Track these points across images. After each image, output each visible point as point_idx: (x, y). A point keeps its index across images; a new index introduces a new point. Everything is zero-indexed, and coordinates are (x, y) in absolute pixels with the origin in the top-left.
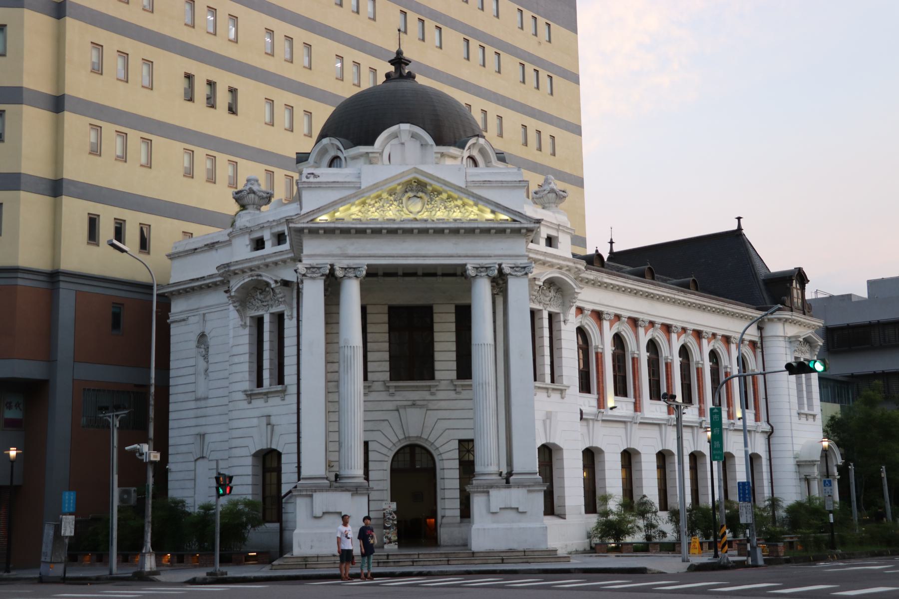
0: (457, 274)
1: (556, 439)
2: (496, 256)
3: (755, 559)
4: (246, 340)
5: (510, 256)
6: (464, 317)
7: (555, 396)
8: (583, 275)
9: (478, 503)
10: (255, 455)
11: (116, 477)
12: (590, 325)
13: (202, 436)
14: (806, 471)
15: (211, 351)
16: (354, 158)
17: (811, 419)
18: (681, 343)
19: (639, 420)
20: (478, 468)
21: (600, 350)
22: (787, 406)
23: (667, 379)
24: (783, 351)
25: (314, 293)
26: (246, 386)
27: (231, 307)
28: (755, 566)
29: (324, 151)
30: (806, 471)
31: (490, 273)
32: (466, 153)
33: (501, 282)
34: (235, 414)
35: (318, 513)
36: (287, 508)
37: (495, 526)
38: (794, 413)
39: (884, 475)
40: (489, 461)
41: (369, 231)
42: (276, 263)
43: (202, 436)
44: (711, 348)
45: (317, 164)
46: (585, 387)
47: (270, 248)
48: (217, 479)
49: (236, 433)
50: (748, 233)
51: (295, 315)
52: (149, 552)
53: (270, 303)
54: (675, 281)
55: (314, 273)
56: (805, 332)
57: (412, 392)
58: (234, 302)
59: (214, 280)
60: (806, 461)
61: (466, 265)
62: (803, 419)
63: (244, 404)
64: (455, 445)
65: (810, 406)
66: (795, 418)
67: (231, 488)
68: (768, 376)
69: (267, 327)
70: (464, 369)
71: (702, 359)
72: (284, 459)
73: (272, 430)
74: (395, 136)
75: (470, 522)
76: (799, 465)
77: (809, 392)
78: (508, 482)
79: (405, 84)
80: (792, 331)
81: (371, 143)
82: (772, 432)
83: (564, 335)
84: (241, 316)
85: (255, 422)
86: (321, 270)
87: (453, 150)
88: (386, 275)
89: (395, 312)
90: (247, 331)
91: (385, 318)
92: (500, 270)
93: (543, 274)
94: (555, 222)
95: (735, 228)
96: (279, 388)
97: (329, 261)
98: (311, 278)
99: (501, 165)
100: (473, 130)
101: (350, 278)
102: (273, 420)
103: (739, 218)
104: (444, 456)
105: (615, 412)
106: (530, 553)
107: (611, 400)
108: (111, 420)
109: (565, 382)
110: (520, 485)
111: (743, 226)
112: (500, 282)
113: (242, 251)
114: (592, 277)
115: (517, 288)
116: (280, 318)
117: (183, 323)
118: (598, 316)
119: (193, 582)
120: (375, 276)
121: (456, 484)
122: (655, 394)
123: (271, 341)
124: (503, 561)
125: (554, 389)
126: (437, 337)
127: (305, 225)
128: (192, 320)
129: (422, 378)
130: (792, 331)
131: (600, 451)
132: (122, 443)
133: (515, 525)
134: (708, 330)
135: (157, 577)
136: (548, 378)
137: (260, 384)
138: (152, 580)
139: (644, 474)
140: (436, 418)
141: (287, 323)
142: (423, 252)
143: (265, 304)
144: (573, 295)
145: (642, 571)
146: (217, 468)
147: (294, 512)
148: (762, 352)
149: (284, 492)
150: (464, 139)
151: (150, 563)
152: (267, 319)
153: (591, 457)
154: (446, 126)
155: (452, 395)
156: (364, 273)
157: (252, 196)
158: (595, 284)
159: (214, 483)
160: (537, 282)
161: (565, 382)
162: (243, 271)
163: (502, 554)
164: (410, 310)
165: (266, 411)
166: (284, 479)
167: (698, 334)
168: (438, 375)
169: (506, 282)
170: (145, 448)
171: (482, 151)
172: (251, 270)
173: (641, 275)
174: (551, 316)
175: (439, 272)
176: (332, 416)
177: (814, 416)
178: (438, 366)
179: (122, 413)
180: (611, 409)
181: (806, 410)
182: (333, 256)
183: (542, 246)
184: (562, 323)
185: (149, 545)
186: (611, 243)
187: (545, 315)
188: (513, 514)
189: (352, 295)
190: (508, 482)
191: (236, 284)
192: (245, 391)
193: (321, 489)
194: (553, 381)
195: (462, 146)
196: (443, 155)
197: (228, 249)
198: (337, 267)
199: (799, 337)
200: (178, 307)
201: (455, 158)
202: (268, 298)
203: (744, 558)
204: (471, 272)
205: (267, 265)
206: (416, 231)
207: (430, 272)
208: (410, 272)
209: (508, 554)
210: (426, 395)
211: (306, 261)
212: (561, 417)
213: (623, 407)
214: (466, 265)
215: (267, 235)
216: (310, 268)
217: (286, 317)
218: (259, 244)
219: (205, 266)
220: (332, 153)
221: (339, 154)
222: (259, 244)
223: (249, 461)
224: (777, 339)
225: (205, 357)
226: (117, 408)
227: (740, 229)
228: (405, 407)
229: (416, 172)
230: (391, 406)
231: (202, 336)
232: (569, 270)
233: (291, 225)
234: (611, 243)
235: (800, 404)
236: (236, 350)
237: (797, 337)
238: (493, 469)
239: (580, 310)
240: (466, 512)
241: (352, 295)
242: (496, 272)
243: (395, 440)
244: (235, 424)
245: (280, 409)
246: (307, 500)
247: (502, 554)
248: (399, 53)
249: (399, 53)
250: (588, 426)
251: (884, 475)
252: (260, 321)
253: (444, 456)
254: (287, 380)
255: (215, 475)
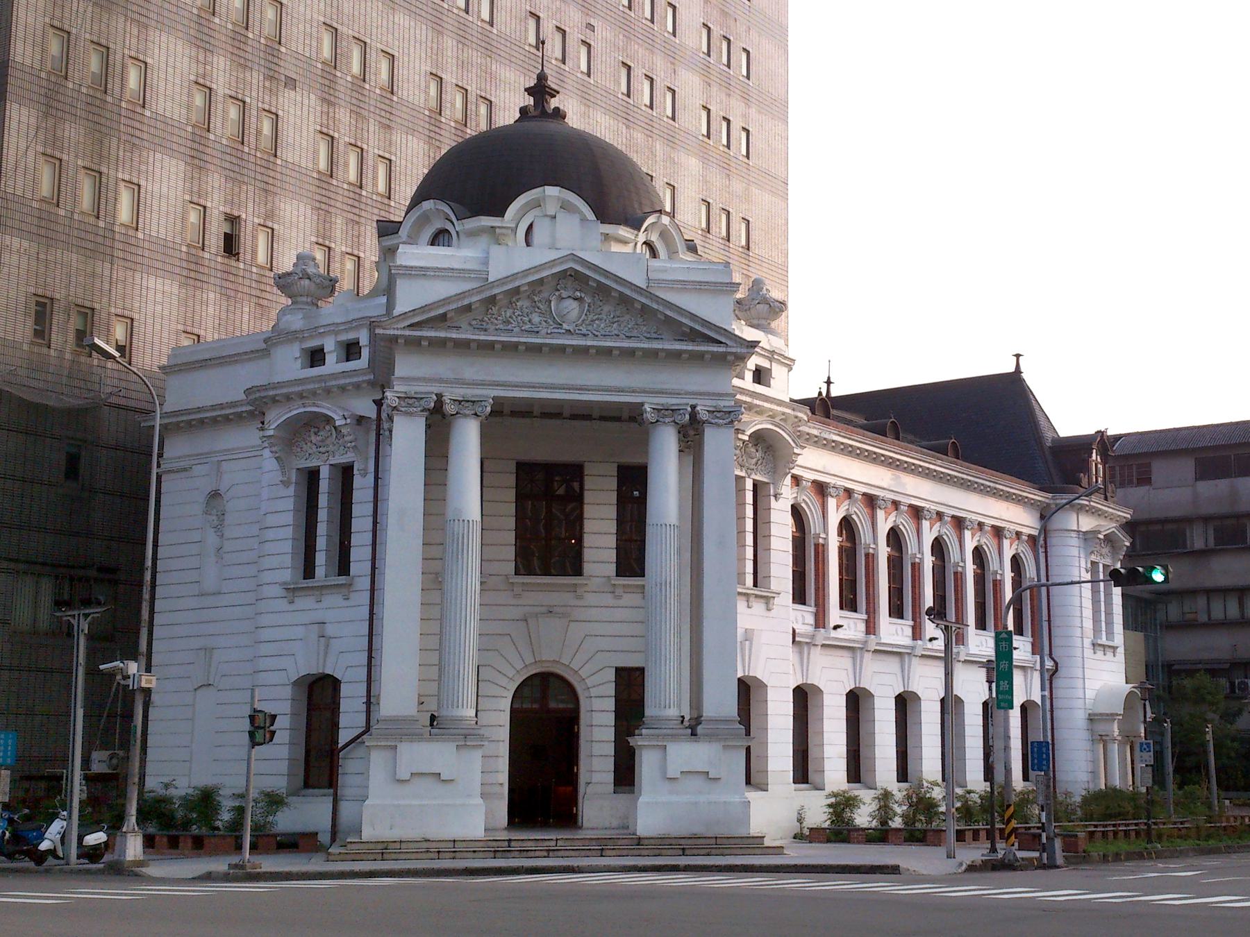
0: (628, 419)
1: (759, 670)
2: (687, 393)
3: (1052, 857)
4: (289, 504)
5: (709, 394)
6: (633, 484)
7: (758, 607)
8: (804, 429)
9: (647, 764)
10: (297, 683)
11: (80, 713)
12: (988, 542)
13: (208, 650)
14: (1101, 728)
15: (229, 519)
16: (473, 234)
17: (1110, 654)
18: (934, 535)
19: (873, 647)
20: (649, 711)
21: (821, 541)
22: (1078, 632)
23: (913, 587)
24: (1075, 552)
25: (408, 437)
26: (286, 575)
27: (267, 453)
28: (1052, 866)
29: (425, 219)
30: (1101, 728)
31: (678, 419)
32: (642, 237)
33: (692, 433)
34: (265, 620)
35: (404, 774)
36: (349, 766)
37: (674, 798)
38: (1087, 643)
39: (1209, 737)
40: (666, 698)
41: (497, 346)
42: (343, 389)
43: (208, 650)
44: (975, 544)
45: (412, 240)
46: (799, 597)
47: (332, 363)
48: (252, 718)
49: (265, 649)
50: (1029, 377)
51: (372, 468)
52: (134, 831)
53: (331, 448)
54: (924, 443)
55: (410, 405)
56: (1108, 527)
57: (547, 591)
58: (271, 445)
59: (239, 410)
60: (1101, 714)
61: (642, 404)
62: (1100, 653)
63: (283, 604)
64: (611, 675)
65: (1110, 634)
66: (1088, 652)
67: (273, 733)
68: (1054, 590)
69: (324, 485)
70: (631, 559)
71: (963, 560)
72: (345, 690)
73: (327, 646)
74: (537, 204)
75: (633, 792)
76: (1092, 719)
77: (1109, 614)
78: (694, 734)
79: (552, 126)
80: (1087, 523)
81: (500, 213)
82: (1057, 670)
83: (774, 516)
84: (282, 467)
85: (300, 632)
86: (422, 402)
87: (624, 231)
88: (546, 415)
89: (525, 470)
90: (291, 491)
91: (511, 480)
92: (693, 415)
93: (752, 424)
94: (767, 347)
95: (1012, 369)
96: (342, 580)
97: (436, 389)
98: (407, 413)
99: (689, 257)
100: (652, 203)
101: (466, 416)
102: (330, 630)
103: (1018, 356)
104: (593, 692)
105: (839, 634)
106: (725, 841)
107: (835, 613)
108: (75, 622)
109: (774, 586)
110: (712, 737)
111: (1023, 369)
112: (691, 435)
113: (287, 365)
114: (815, 432)
115: (716, 442)
116: (346, 473)
117: (183, 474)
118: (821, 489)
119: (208, 877)
120: (504, 417)
121: (610, 734)
122: (849, 603)
123: (329, 508)
124: (684, 852)
125: (757, 596)
126: (588, 511)
127: (399, 332)
128: (198, 470)
129: (564, 574)
130: (1087, 523)
131: (818, 691)
132: (95, 656)
133: (702, 799)
134: (974, 517)
135: (144, 870)
136: (749, 580)
137: (309, 572)
138: (137, 875)
139: (878, 726)
140: (589, 632)
141: (358, 481)
142: (579, 382)
143: (322, 450)
144: (790, 460)
145: (895, 870)
146: (252, 703)
147: (365, 774)
148: (1046, 552)
149: (342, 741)
150: (639, 214)
151: (133, 847)
152: (324, 473)
153: (804, 698)
154: (609, 189)
155: (608, 599)
156: (489, 409)
157: (307, 282)
158: (818, 442)
159: (246, 725)
160: (740, 436)
161: (774, 587)
162: (288, 398)
163: (683, 842)
164: (550, 470)
165: (319, 616)
166: (344, 720)
167: (959, 523)
168: (588, 568)
169: (700, 434)
170: (133, 668)
171: (664, 235)
172: (302, 397)
173: (880, 431)
174: (756, 485)
175: (596, 414)
176: (438, 626)
177: (1114, 648)
178: (588, 554)
179: (96, 612)
180: (836, 628)
181: (1103, 640)
182: (441, 381)
183: (747, 382)
184: (772, 499)
185: (133, 819)
186: (829, 382)
187: (749, 485)
188: (698, 782)
189: (468, 441)
190: (694, 734)
191: (276, 418)
192: (285, 583)
193: (415, 737)
194: (755, 585)
195: (636, 225)
196: (607, 237)
197: (264, 363)
198: (446, 399)
199: (1100, 532)
200: (177, 449)
201: (624, 242)
202: (328, 441)
203: (1036, 854)
204: (650, 416)
205: (328, 391)
206: (569, 350)
207: (582, 414)
208: (552, 412)
209: (690, 842)
210: (567, 598)
211: (399, 388)
212: (770, 640)
213: (851, 627)
214: (642, 404)
215: (329, 345)
216: (405, 398)
217: (355, 472)
218: (316, 357)
219: (225, 387)
220: (438, 224)
221: (449, 227)
222: (316, 357)
223: (287, 692)
224: (1067, 534)
225: (219, 529)
226: (87, 603)
227: (1018, 370)
228: (536, 615)
229: (574, 261)
230: (517, 613)
231: (215, 495)
232: (784, 420)
233: (378, 331)
234: (829, 382)
235: (1097, 630)
236: (271, 520)
237: (1094, 532)
238: (673, 712)
239: (797, 480)
240: (625, 776)
241: (468, 441)
242: (687, 417)
243: (519, 665)
244: (266, 634)
245: (342, 614)
246: (388, 754)
247: (683, 842)
248: (542, 77)
249: (542, 77)
250: (801, 653)
251: (1209, 737)
252: (312, 476)
253: (593, 692)
254: (354, 568)
255: (248, 712)
